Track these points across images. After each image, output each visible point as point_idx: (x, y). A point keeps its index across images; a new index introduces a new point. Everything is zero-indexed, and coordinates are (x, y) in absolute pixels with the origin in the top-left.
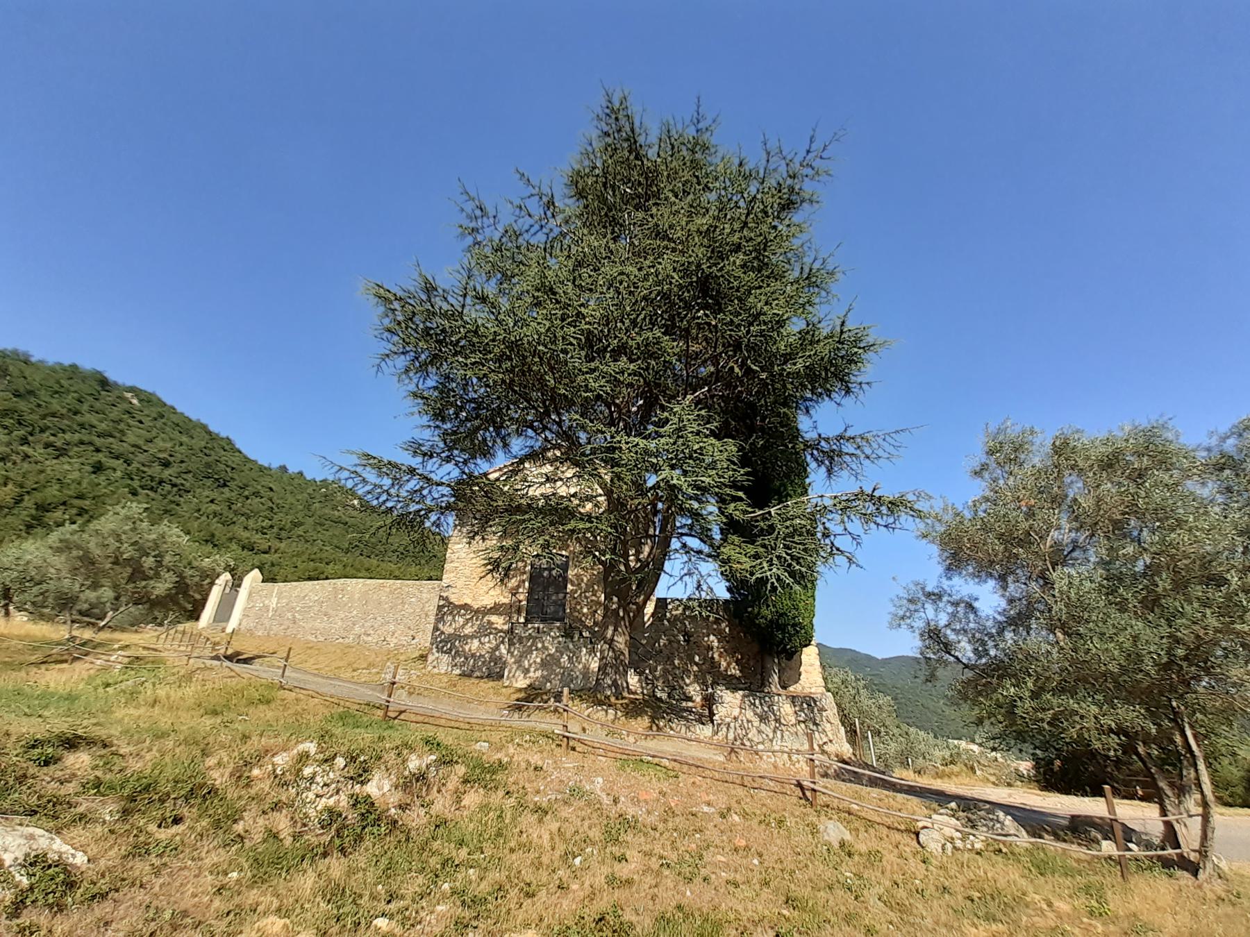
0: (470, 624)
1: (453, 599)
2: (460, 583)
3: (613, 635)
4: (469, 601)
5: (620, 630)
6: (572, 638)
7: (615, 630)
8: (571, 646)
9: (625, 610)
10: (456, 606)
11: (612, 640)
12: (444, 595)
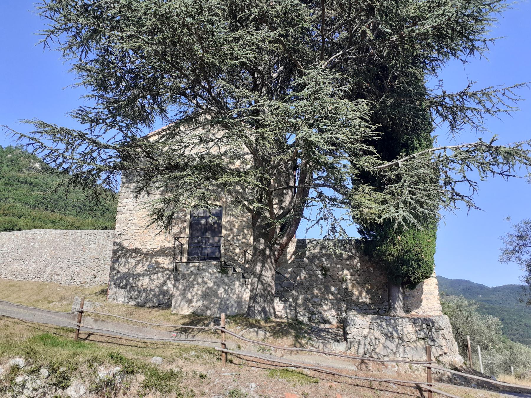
0: (141, 265)
1: (125, 244)
2: (130, 231)
3: (261, 271)
4: (139, 246)
5: (267, 266)
6: (227, 273)
7: (263, 266)
8: (226, 280)
9: (271, 250)
10: (128, 251)
11: (261, 274)
12: (118, 241)
